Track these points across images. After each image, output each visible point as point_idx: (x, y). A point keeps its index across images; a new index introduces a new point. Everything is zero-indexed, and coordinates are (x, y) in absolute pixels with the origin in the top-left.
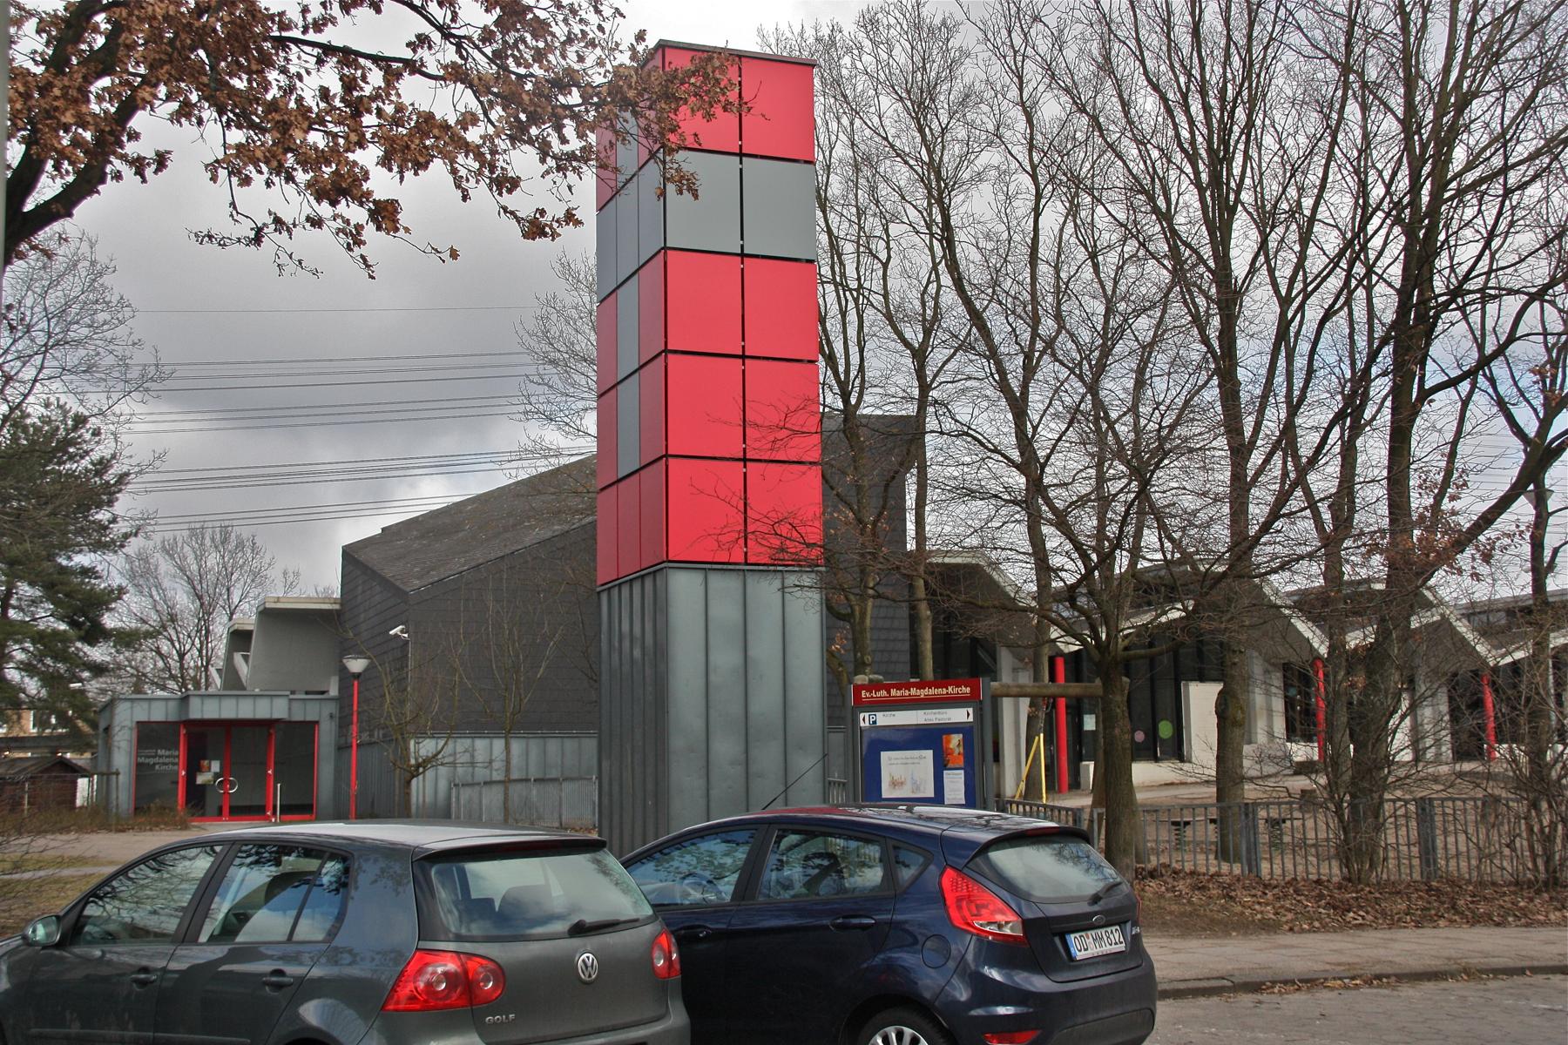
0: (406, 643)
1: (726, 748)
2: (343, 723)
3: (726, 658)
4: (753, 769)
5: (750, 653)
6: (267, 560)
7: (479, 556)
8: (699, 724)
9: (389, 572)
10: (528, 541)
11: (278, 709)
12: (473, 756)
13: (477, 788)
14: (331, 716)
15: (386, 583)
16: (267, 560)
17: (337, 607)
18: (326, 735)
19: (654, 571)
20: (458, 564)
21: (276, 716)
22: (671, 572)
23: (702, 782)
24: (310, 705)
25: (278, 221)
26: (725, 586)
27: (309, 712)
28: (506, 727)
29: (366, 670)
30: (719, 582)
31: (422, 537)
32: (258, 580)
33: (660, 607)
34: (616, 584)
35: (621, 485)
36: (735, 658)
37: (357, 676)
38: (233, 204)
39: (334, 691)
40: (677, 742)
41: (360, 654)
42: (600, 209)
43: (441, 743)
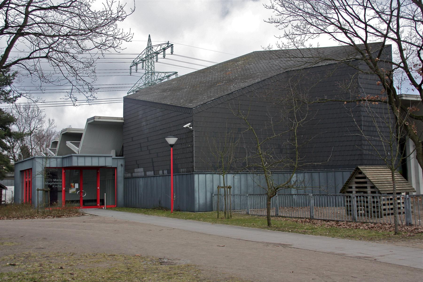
17: (123, 121)
18: (120, 173)
29: (176, 143)
37: (172, 146)
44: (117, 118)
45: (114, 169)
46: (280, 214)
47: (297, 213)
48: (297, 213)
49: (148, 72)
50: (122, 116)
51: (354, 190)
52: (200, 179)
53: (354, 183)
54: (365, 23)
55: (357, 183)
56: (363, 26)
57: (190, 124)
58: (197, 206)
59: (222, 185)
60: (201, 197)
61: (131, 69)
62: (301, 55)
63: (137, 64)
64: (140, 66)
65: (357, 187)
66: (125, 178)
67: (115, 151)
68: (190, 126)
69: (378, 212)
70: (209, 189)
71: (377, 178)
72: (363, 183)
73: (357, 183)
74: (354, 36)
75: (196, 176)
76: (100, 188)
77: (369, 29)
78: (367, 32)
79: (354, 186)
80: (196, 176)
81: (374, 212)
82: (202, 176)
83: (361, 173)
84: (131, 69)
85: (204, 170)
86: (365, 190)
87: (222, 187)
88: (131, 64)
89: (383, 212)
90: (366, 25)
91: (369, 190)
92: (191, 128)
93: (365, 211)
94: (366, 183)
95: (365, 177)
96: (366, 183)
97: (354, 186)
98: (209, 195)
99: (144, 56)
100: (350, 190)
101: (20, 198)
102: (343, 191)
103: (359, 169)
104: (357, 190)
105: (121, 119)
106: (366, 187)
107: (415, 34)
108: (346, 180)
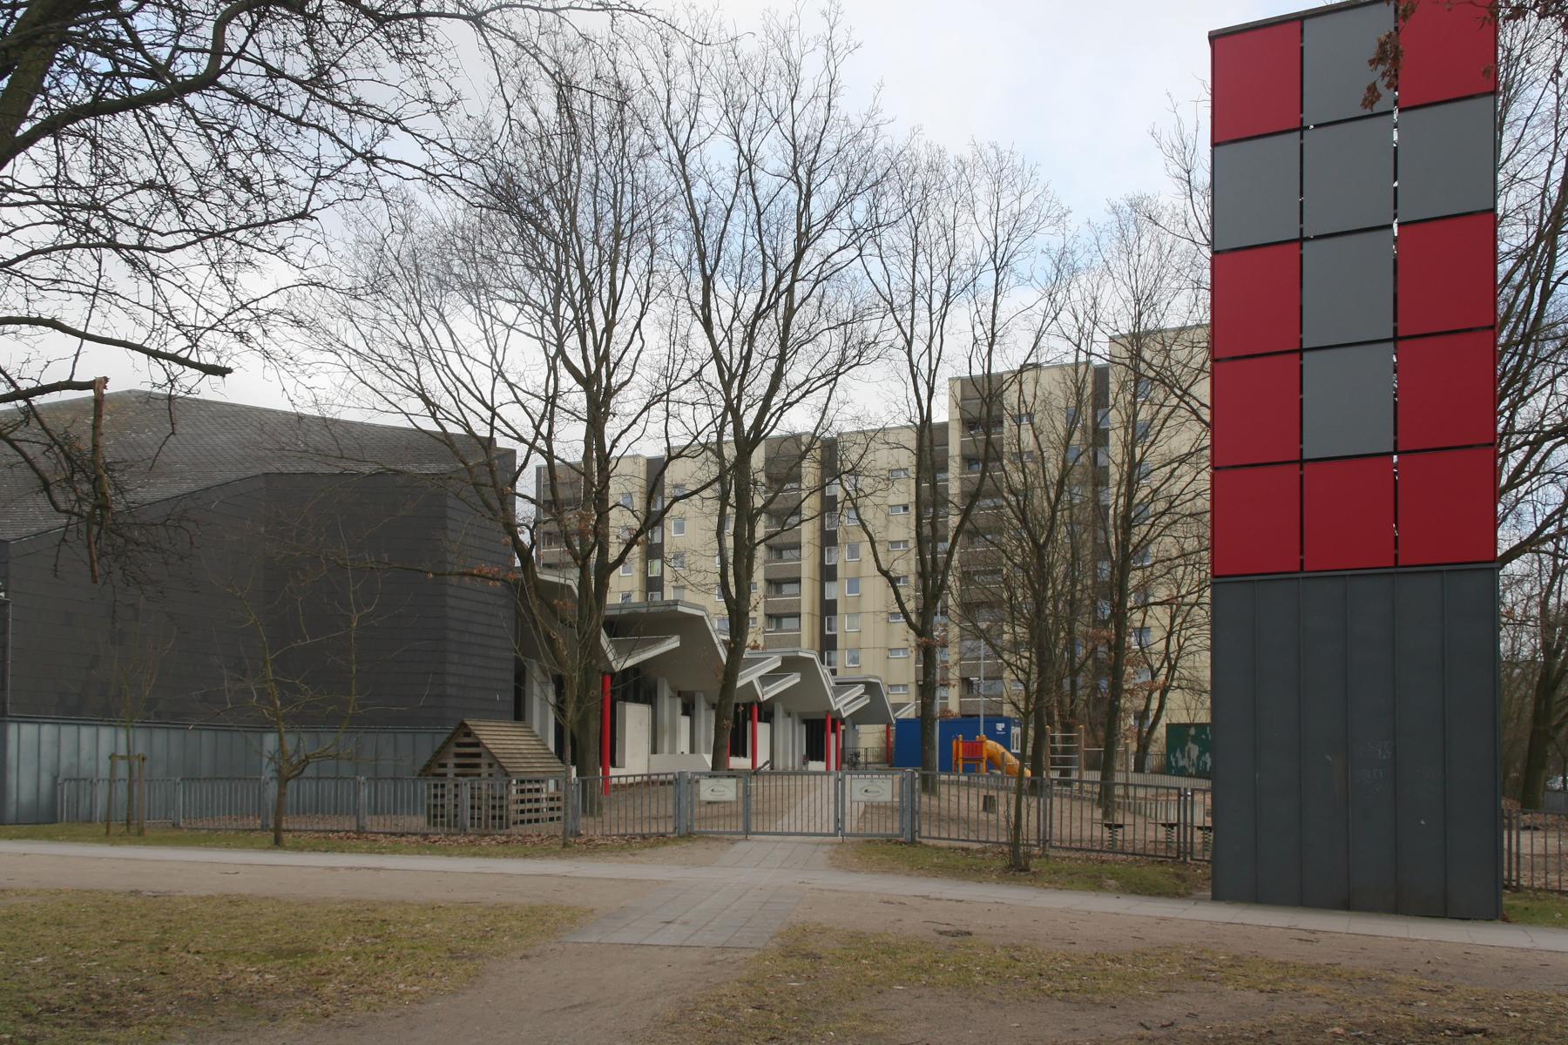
47: (654, 806)
48: (654, 806)
51: (451, 771)
52: (23, 737)
54: (492, 409)
55: (458, 755)
56: (487, 414)
58: (12, 810)
59: (122, 751)
60: (24, 785)
62: (338, 453)
65: (457, 766)
69: (501, 818)
70: (46, 762)
72: (471, 756)
73: (458, 755)
74: (724, 585)
75: (12, 729)
77: (497, 422)
78: (493, 428)
79: (451, 762)
80: (12, 729)
81: (494, 818)
82: (28, 730)
83: (468, 734)
85: (34, 714)
86: (476, 771)
87: (122, 758)
89: (513, 816)
90: (494, 414)
91: (484, 770)
94: (478, 755)
95: (478, 744)
96: (478, 755)
97: (451, 762)
98: (46, 780)
100: (442, 770)
102: (426, 771)
103: (466, 726)
104: (459, 770)
106: (477, 766)
108: (438, 745)
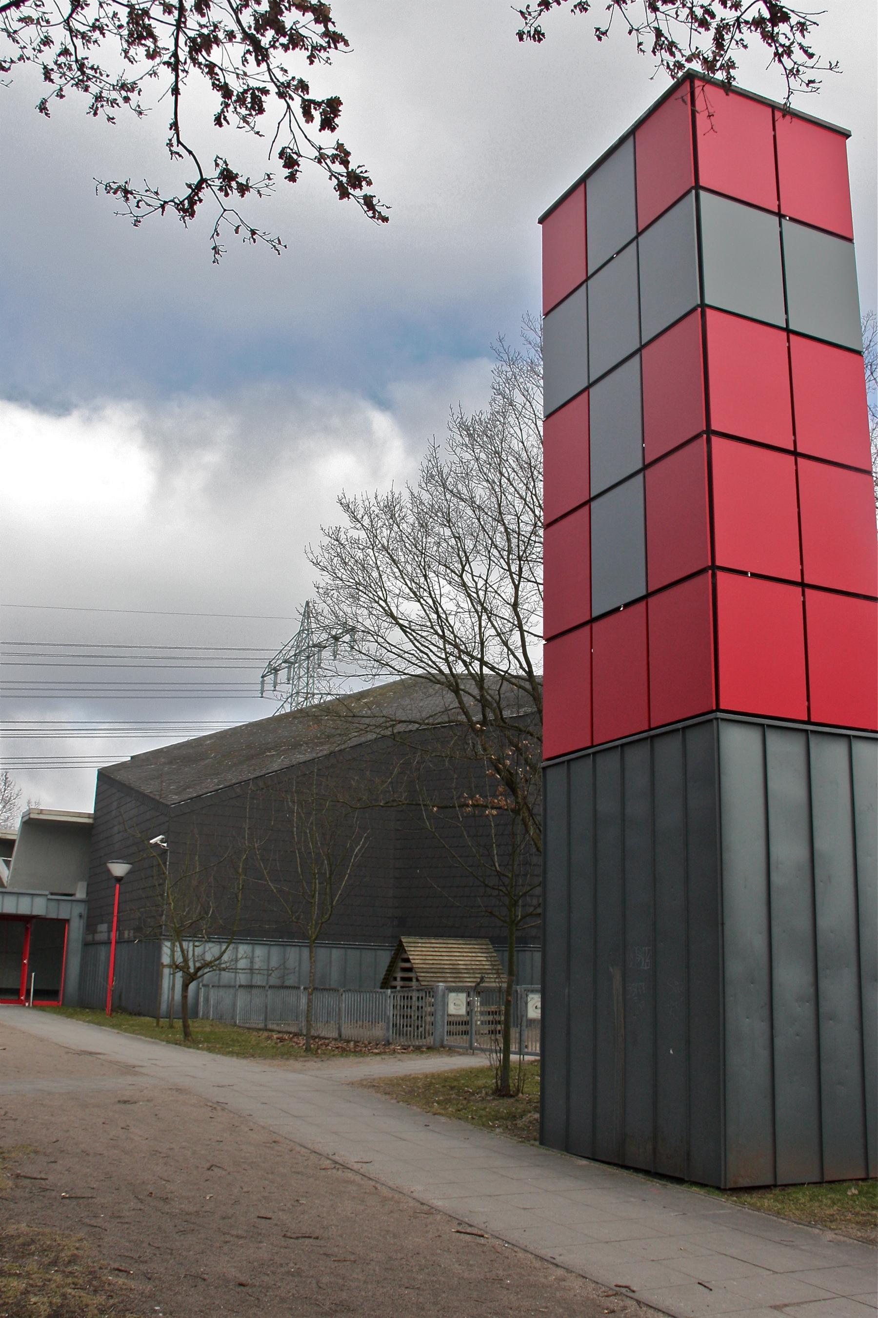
0: (164, 852)
1: (792, 977)
2: (90, 927)
3: (789, 851)
4: (824, 1008)
5: (817, 845)
6: (16, 790)
7: (232, 777)
8: (759, 942)
9: (147, 789)
10: (276, 767)
11: (38, 907)
12: (252, 962)
13: (232, 991)
14: (81, 916)
15: (143, 798)
16: (16, 790)
17: (90, 821)
18: (75, 932)
19: (707, 718)
20: (211, 785)
21: (35, 913)
22: (723, 726)
23: (764, 1026)
24: (63, 905)
25: (228, 176)
26: (785, 748)
27: (63, 912)
28: (281, 933)
29: (129, 873)
30: (779, 744)
31: (171, 763)
32: (8, 807)
33: (710, 774)
34: (566, 760)
35: (595, 626)
36: (800, 852)
37: (119, 879)
38: (175, 126)
39: (81, 894)
40: (735, 968)
41: (122, 858)
42: (546, 314)
43: (224, 947)
44: (80, 815)
45: (62, 924)
46: (270, 1026)
49: (298, 693)
50: (93, 812)
53: (399, 970)
57: (161, 837)
58: (164, 1006)
61: (263, 683)
63: (276, 670)
64: (283, 675)
66: (86, 944)
67: (85, 884)
68: (162, 841)
71: (431, 962)
76: (28, 962)
84: (263, 683)
88: (261, 672)
92: (165, 845)
93: (388, 1023)
99: (292, 653)
101: (166, 996)
105: (89, 816)
107: (468, 686)
